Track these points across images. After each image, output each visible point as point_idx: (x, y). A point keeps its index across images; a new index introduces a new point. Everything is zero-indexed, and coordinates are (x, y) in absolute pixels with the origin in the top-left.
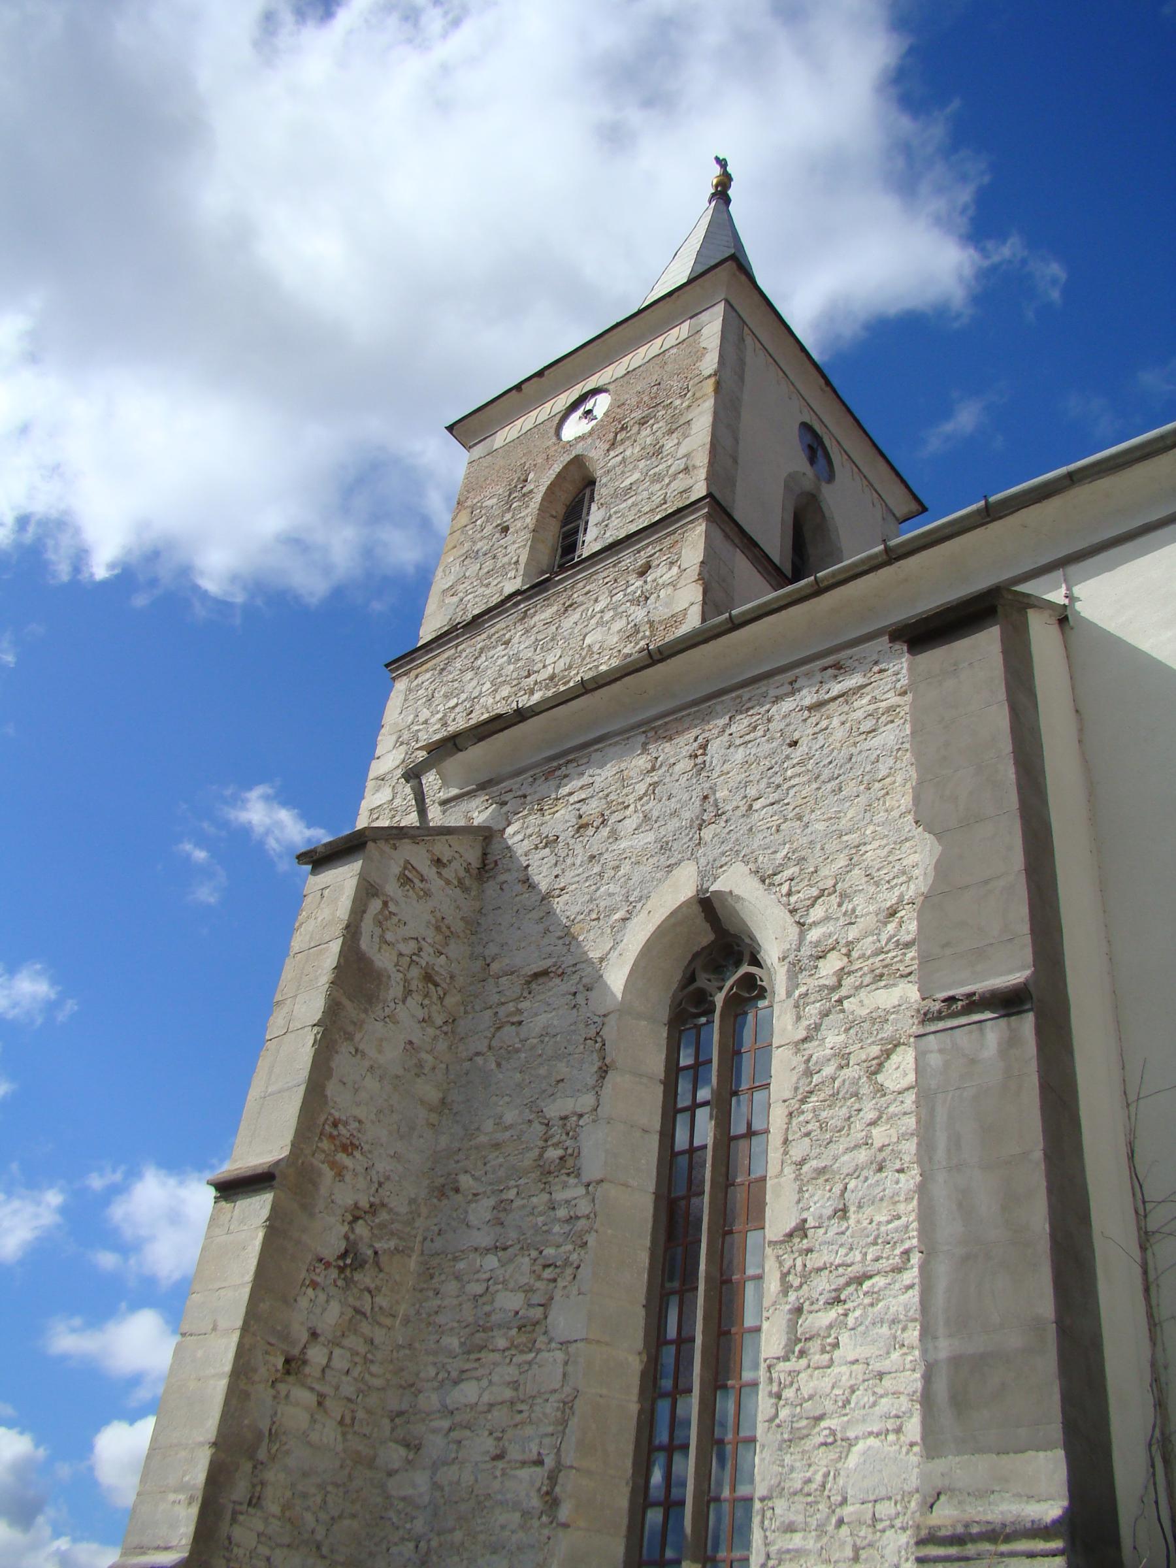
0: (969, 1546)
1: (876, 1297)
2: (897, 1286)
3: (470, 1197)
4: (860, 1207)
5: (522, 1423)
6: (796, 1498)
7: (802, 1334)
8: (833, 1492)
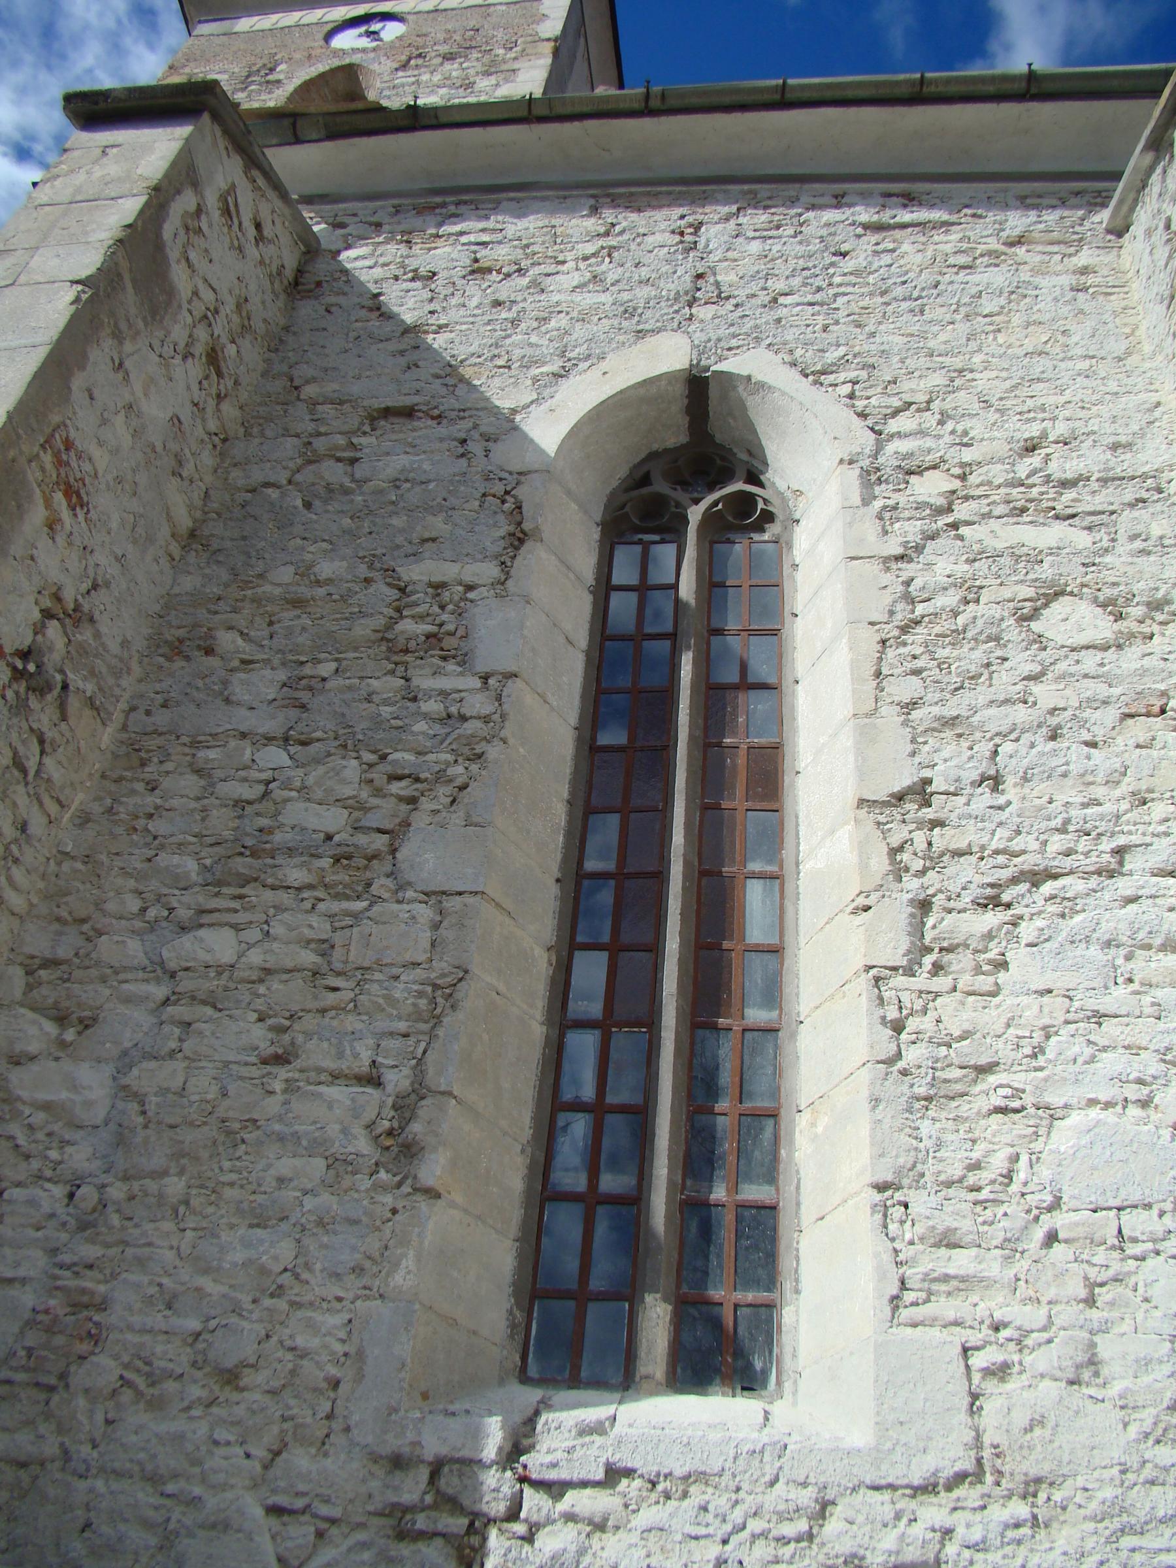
1: (1068, 906)
2: (1107, 895)
3: (236, 663)
4: (1025, 779)
5: (339, 1009)
6: (951, 1192)
8: (1031, 1187)
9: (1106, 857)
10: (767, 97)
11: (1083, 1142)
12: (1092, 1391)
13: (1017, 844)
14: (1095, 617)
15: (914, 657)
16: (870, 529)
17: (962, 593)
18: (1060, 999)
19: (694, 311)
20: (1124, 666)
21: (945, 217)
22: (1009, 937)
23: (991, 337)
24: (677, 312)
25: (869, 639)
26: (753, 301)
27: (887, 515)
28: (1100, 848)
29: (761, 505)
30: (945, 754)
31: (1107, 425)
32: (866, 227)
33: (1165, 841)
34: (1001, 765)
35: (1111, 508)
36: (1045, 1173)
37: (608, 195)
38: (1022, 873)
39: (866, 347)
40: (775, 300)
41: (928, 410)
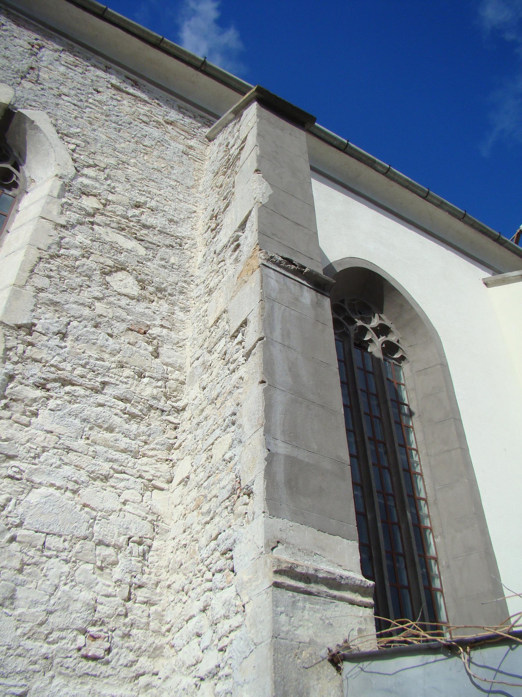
0: (312, 585)
1: (74, 399)
2: (92, 400)
4: (77, 339)
7: (9, 394)
8: (12, 514)
9: (98, 384)
10: (96, 10)
11: (42, 501)
12: (7, 611)
13: (62, 365)
14: (134, 285)
15: (51, 270)
16: (55, 209)
17: (83, 252)
18: (55, 437)
19: (23, 81)
20: (137, 309)
21: (147, 99)
22: (43, 403)
23: (142, 155)
24: (14, 78)
25: (35, 254)
26: (51, 91)
27: (66, 206)
28: (97, 379)
29: (14, 179)
30: (47, 316)
31: (172, 211)
32: (113, 85)
33: (124, 386)
34: (69, 330)
35: (159, 244)
36: (20, 510)
37: (7, 11)
38: (60, 378)
39: (89, 134)
40: (60, 95)
41: (103, 171)
